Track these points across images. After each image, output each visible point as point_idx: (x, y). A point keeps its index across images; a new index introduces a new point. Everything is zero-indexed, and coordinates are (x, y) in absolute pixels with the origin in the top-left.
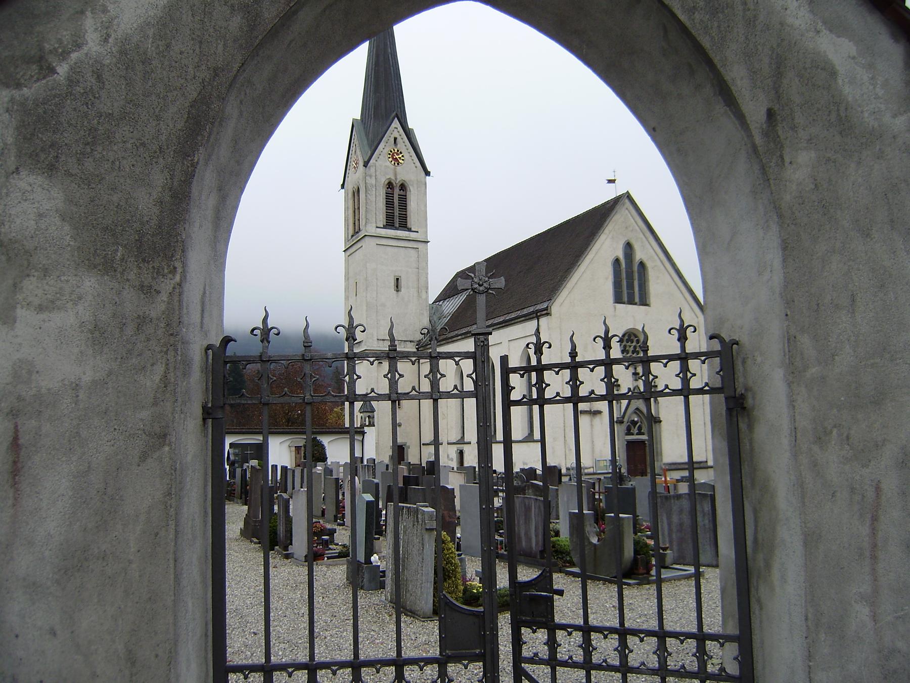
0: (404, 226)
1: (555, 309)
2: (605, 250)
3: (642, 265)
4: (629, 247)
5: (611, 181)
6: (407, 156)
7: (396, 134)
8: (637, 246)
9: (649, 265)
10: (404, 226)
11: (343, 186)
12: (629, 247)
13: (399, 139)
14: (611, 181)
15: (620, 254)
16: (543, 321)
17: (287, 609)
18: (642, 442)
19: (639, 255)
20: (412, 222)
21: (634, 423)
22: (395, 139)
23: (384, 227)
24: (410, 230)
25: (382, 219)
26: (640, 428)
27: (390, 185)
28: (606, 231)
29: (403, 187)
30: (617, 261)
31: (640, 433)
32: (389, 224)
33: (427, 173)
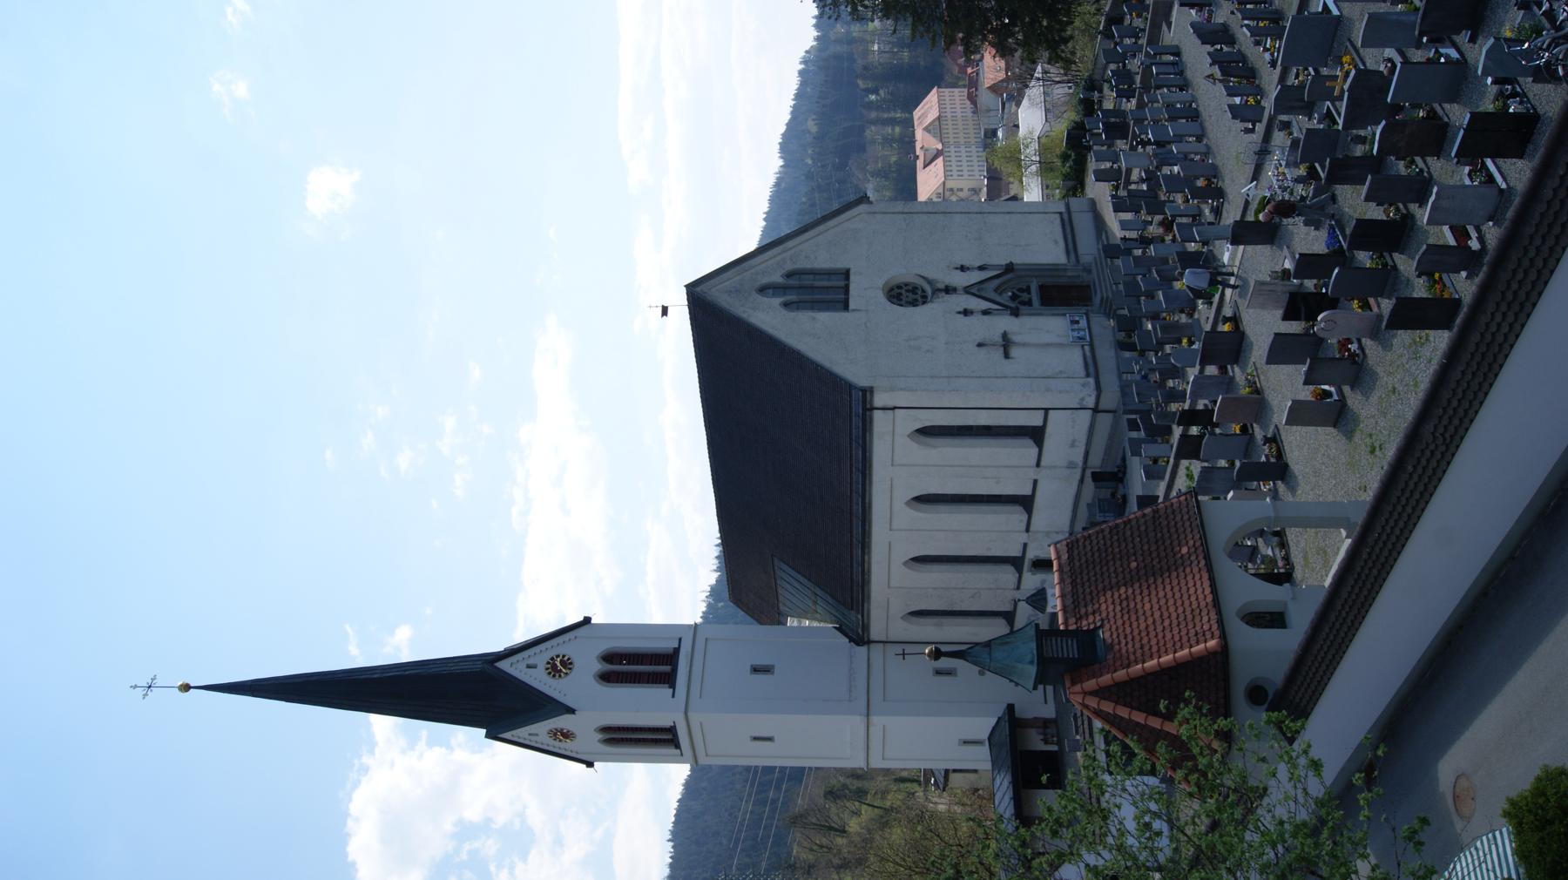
0: (671, 658)
1: (862, 382)
2: (770, 317)
3: (789, 275)
4: (762, 290)
5: (665, 311)
6: (561, 651)
7: (522, 666)
8: (765, 280)
9: (789, 267)
10: (671, 658)
11: (590, 764)
12: (762, 290)
13: (531, 662)
14: (665, 311)
15: (776, 301)
16: (879, 399)
17: (1499, 134)
18: (1042, 288)
19: (777, 278)
20: (668, 645)
21: (1014, 298)
22: (529, 667)
23: (673, 686)
24: (677, 651)
25: (663, 692)
26: (1021, 290)
27: (606, 678)
28: (745, 316)
29: (609, 657)
30: (786, 305)
31: (1028, 290)
32: (669, 679)
33: (587, 620)
